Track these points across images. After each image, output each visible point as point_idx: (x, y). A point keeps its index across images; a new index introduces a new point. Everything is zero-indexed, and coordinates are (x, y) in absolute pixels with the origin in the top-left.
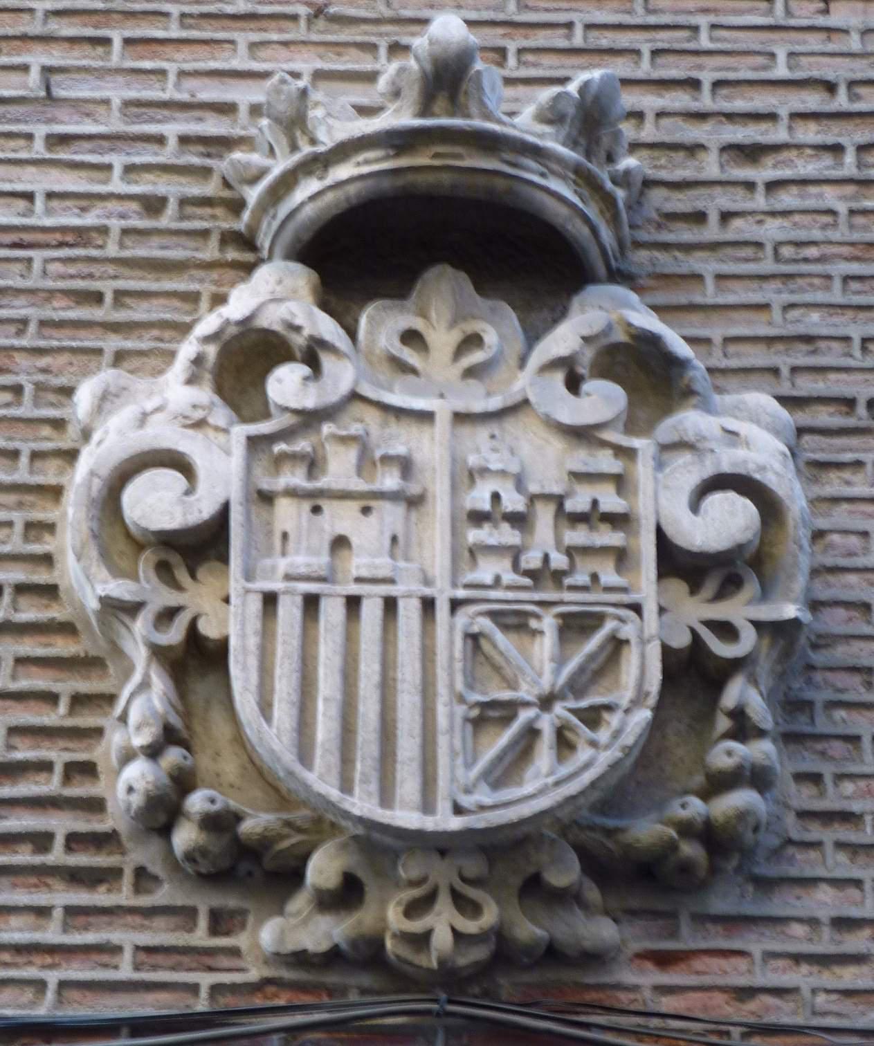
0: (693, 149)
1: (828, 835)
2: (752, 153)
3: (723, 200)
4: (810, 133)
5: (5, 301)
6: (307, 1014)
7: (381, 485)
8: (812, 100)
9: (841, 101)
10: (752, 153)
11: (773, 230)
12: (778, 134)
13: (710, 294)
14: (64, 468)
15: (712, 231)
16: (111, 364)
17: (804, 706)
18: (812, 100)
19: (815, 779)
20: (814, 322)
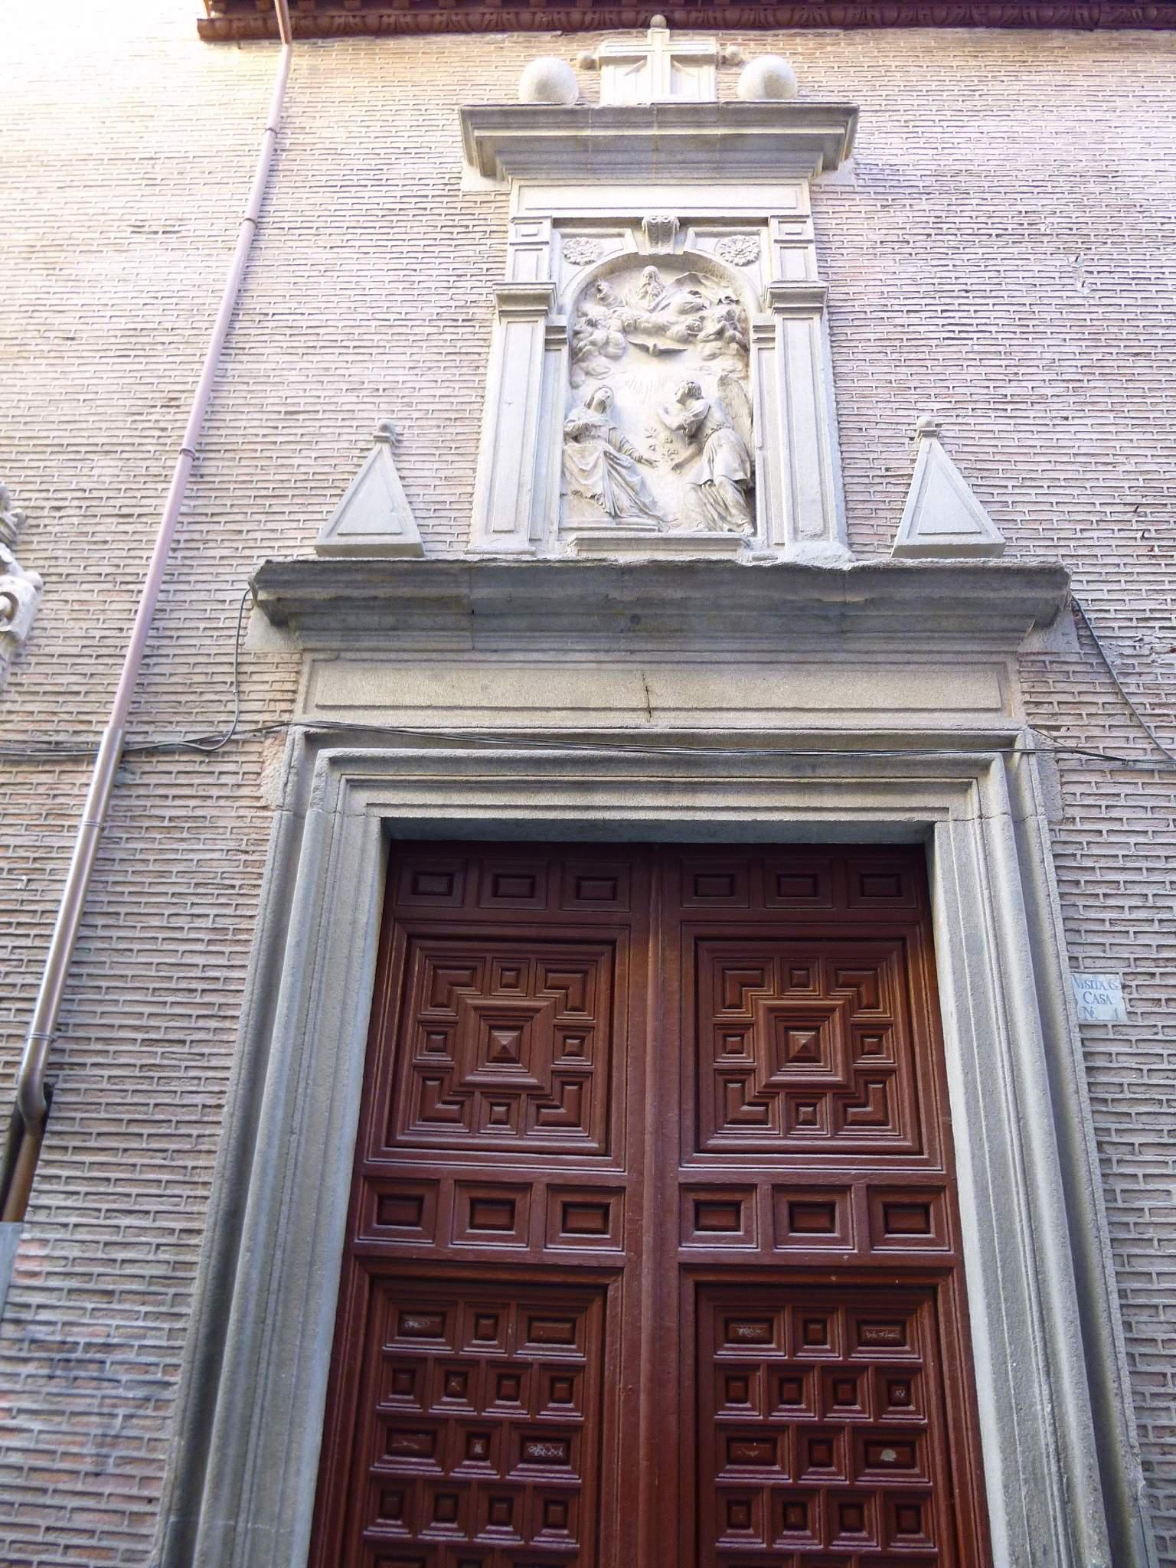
0: (43, 508)
1: (13, 689)
2: (59, 509)
3: (47, 521)
4: (76, 503)
5: (3, 1006)
6: (820, 35)
7: (672, 91)
8: (79, 494)
9: (87, 495)
10: (59, 509)
11: (57, 529)
12: (67, 503)
13: (34, 546)
14: (768, 95)
15: (41, 530)
16: (399, 836)
17: (19, 655)
18: (79, 494)
19: (16, 674)
20: (59, 553)
